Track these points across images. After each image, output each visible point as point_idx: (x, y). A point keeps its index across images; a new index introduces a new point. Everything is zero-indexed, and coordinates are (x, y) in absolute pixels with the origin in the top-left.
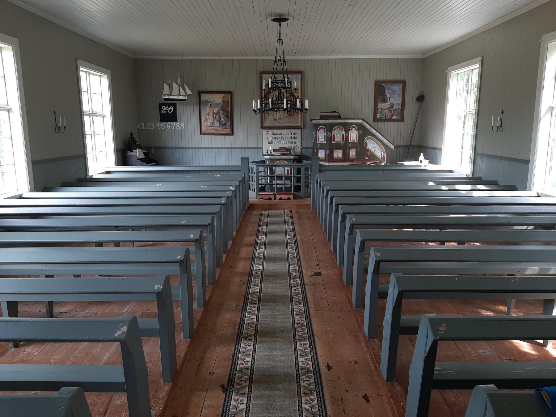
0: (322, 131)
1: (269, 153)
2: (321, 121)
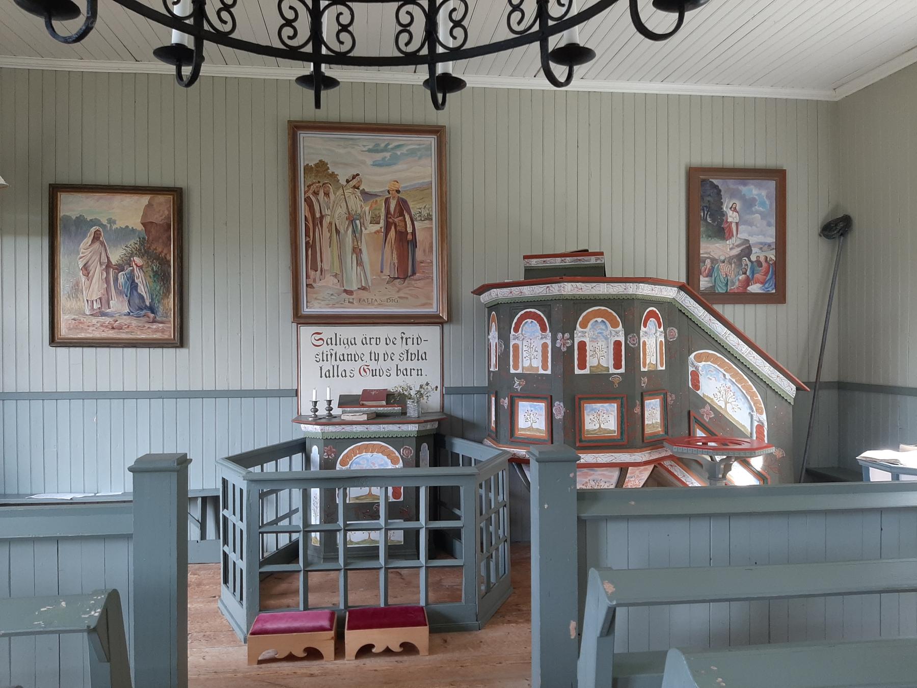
0: (531, 328)
1: (322, 412)
2: (528, 291)
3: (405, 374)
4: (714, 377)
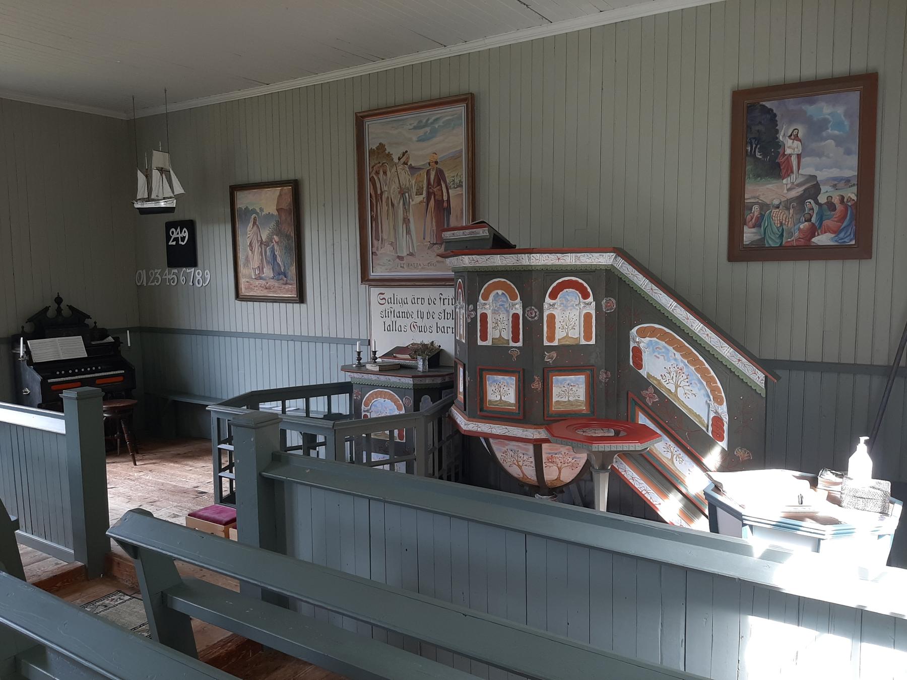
3: (443, 331)
4: (663, 356)
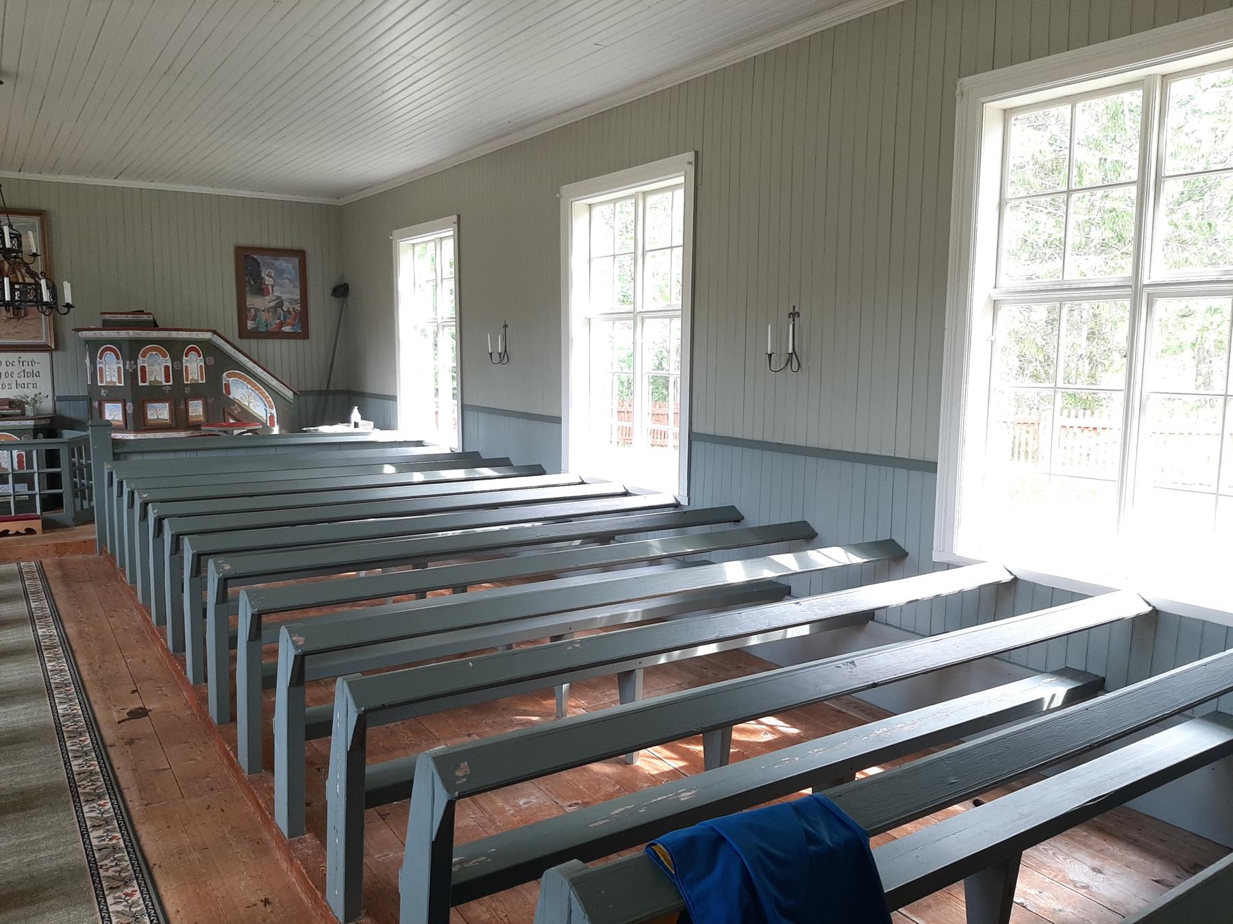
0: (110, 356)
2: (106, 334)
